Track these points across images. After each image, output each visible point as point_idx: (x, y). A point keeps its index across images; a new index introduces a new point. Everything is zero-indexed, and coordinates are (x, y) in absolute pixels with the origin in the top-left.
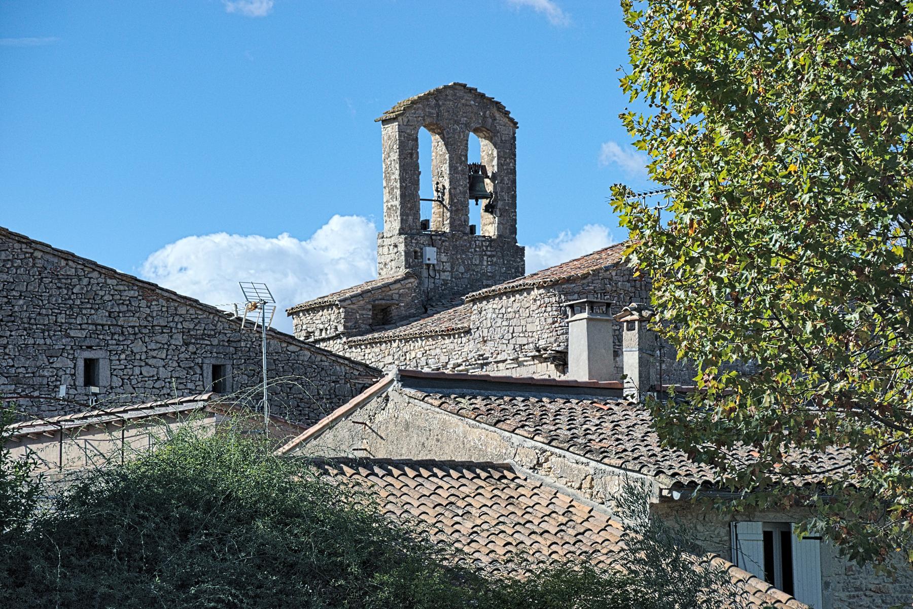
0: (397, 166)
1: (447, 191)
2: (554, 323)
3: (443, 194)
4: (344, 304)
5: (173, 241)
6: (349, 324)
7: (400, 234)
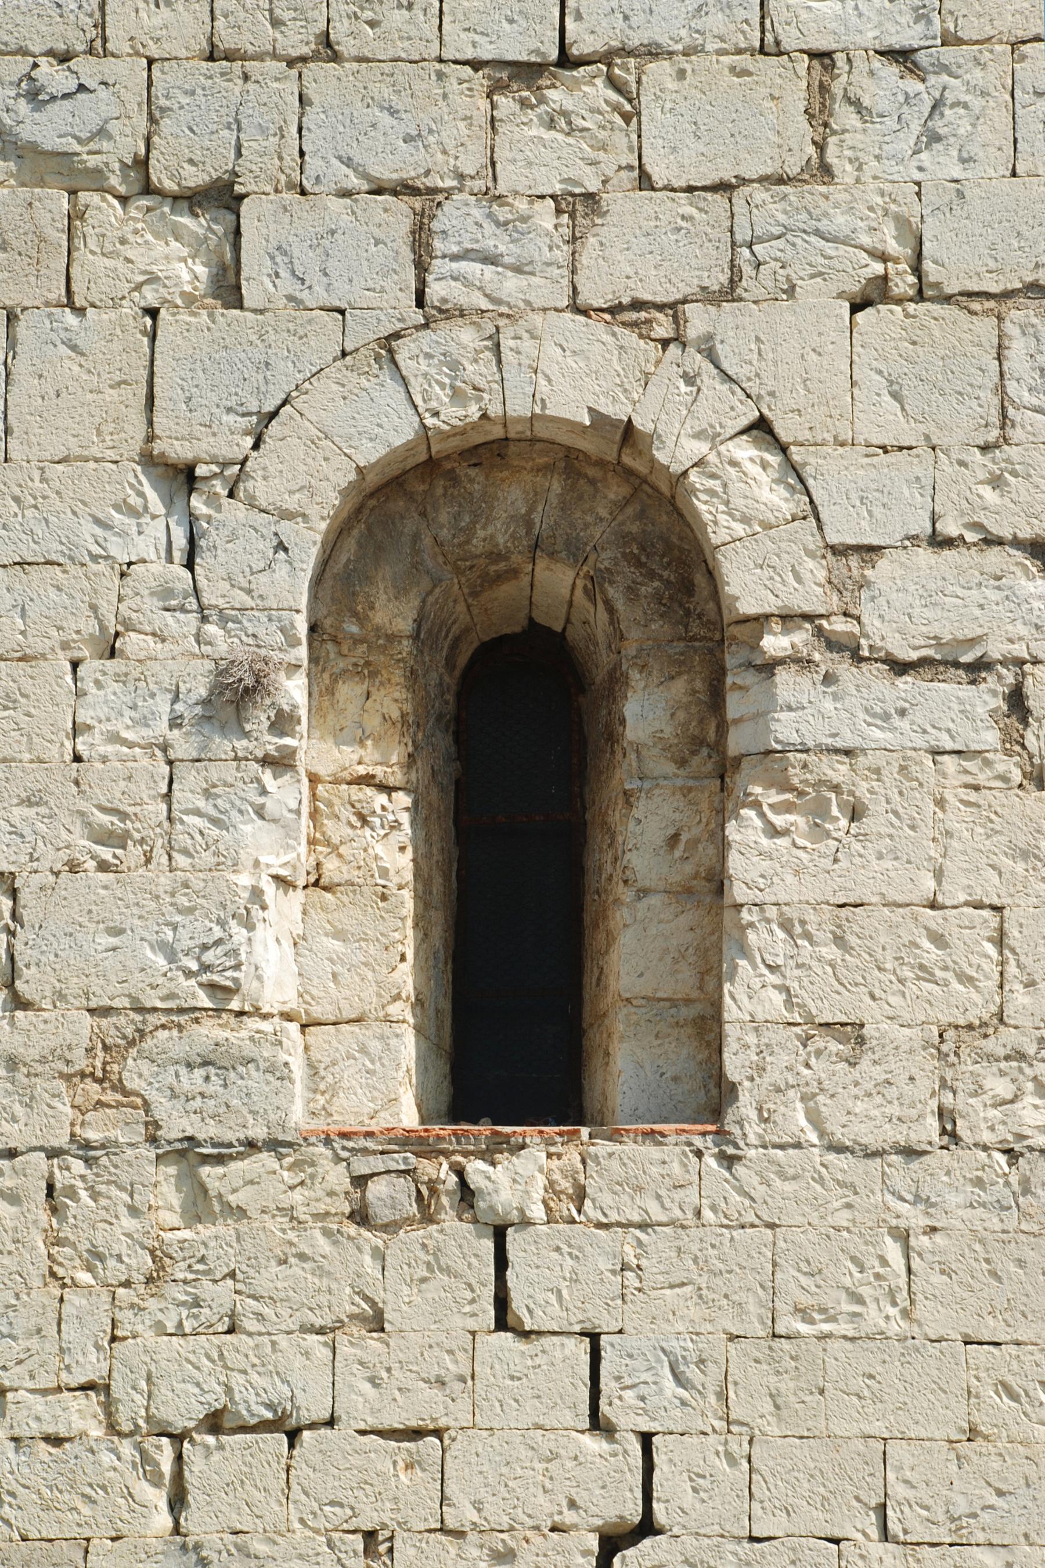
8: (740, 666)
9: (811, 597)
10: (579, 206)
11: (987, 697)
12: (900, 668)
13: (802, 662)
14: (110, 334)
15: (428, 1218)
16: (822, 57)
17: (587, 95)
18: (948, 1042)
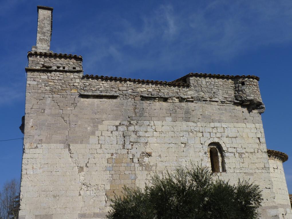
8: (231, 102)
9: (227, 150)
10: (216, 133)
11: (233, 154)
12: (230, 153)
13: (226, 152)
14: (198, 138)
15: (215, 176)
16: (224, 127)
17: (215, 128)
18: (234, 168)
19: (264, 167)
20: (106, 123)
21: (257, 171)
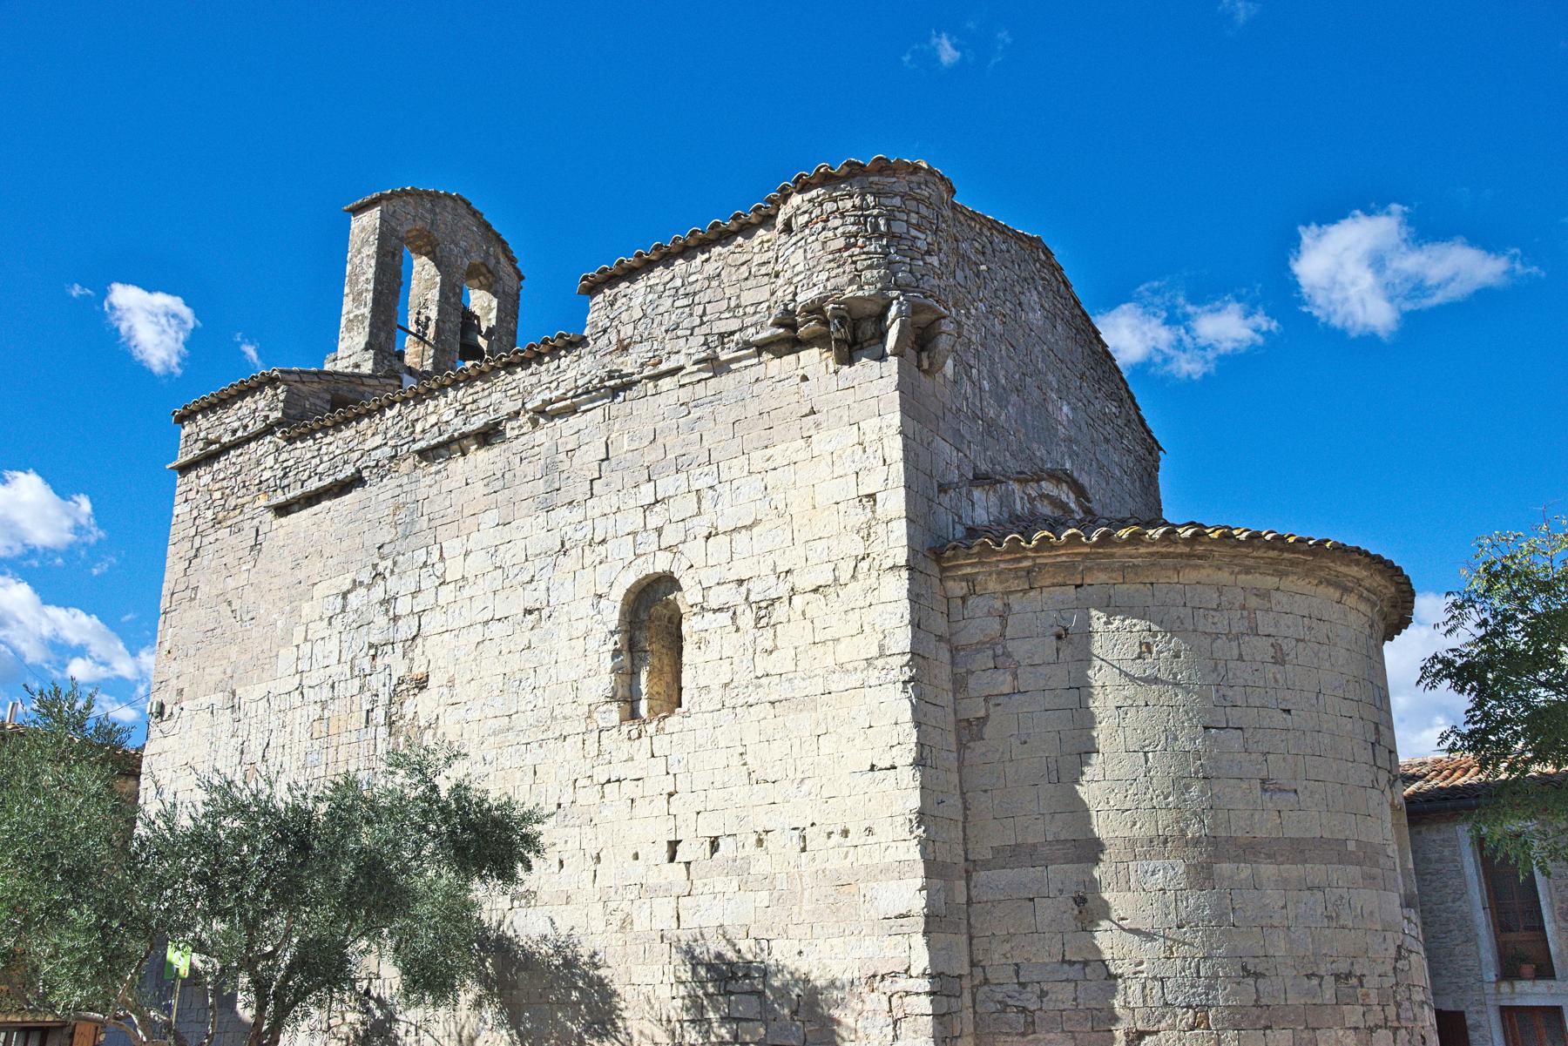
0: (373, 262)
1: (432, 325)
2: (847, 247)
3: (426, 327)
4: (288, 377)
5: (58, 606)
6: (292, 412)
7: (366, 349)
19: (874, 652)
20: (319, 591)
21: (837, 682)
